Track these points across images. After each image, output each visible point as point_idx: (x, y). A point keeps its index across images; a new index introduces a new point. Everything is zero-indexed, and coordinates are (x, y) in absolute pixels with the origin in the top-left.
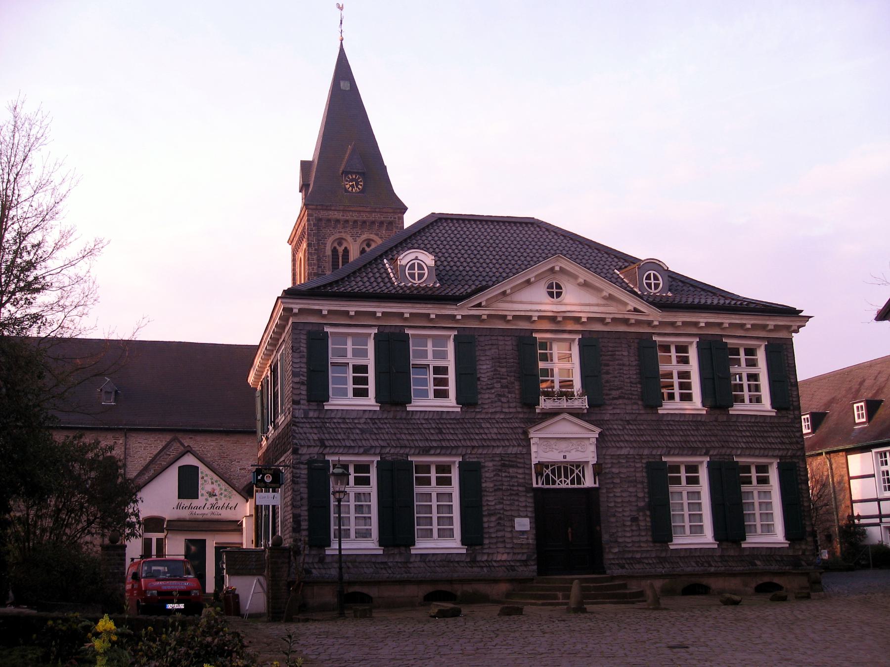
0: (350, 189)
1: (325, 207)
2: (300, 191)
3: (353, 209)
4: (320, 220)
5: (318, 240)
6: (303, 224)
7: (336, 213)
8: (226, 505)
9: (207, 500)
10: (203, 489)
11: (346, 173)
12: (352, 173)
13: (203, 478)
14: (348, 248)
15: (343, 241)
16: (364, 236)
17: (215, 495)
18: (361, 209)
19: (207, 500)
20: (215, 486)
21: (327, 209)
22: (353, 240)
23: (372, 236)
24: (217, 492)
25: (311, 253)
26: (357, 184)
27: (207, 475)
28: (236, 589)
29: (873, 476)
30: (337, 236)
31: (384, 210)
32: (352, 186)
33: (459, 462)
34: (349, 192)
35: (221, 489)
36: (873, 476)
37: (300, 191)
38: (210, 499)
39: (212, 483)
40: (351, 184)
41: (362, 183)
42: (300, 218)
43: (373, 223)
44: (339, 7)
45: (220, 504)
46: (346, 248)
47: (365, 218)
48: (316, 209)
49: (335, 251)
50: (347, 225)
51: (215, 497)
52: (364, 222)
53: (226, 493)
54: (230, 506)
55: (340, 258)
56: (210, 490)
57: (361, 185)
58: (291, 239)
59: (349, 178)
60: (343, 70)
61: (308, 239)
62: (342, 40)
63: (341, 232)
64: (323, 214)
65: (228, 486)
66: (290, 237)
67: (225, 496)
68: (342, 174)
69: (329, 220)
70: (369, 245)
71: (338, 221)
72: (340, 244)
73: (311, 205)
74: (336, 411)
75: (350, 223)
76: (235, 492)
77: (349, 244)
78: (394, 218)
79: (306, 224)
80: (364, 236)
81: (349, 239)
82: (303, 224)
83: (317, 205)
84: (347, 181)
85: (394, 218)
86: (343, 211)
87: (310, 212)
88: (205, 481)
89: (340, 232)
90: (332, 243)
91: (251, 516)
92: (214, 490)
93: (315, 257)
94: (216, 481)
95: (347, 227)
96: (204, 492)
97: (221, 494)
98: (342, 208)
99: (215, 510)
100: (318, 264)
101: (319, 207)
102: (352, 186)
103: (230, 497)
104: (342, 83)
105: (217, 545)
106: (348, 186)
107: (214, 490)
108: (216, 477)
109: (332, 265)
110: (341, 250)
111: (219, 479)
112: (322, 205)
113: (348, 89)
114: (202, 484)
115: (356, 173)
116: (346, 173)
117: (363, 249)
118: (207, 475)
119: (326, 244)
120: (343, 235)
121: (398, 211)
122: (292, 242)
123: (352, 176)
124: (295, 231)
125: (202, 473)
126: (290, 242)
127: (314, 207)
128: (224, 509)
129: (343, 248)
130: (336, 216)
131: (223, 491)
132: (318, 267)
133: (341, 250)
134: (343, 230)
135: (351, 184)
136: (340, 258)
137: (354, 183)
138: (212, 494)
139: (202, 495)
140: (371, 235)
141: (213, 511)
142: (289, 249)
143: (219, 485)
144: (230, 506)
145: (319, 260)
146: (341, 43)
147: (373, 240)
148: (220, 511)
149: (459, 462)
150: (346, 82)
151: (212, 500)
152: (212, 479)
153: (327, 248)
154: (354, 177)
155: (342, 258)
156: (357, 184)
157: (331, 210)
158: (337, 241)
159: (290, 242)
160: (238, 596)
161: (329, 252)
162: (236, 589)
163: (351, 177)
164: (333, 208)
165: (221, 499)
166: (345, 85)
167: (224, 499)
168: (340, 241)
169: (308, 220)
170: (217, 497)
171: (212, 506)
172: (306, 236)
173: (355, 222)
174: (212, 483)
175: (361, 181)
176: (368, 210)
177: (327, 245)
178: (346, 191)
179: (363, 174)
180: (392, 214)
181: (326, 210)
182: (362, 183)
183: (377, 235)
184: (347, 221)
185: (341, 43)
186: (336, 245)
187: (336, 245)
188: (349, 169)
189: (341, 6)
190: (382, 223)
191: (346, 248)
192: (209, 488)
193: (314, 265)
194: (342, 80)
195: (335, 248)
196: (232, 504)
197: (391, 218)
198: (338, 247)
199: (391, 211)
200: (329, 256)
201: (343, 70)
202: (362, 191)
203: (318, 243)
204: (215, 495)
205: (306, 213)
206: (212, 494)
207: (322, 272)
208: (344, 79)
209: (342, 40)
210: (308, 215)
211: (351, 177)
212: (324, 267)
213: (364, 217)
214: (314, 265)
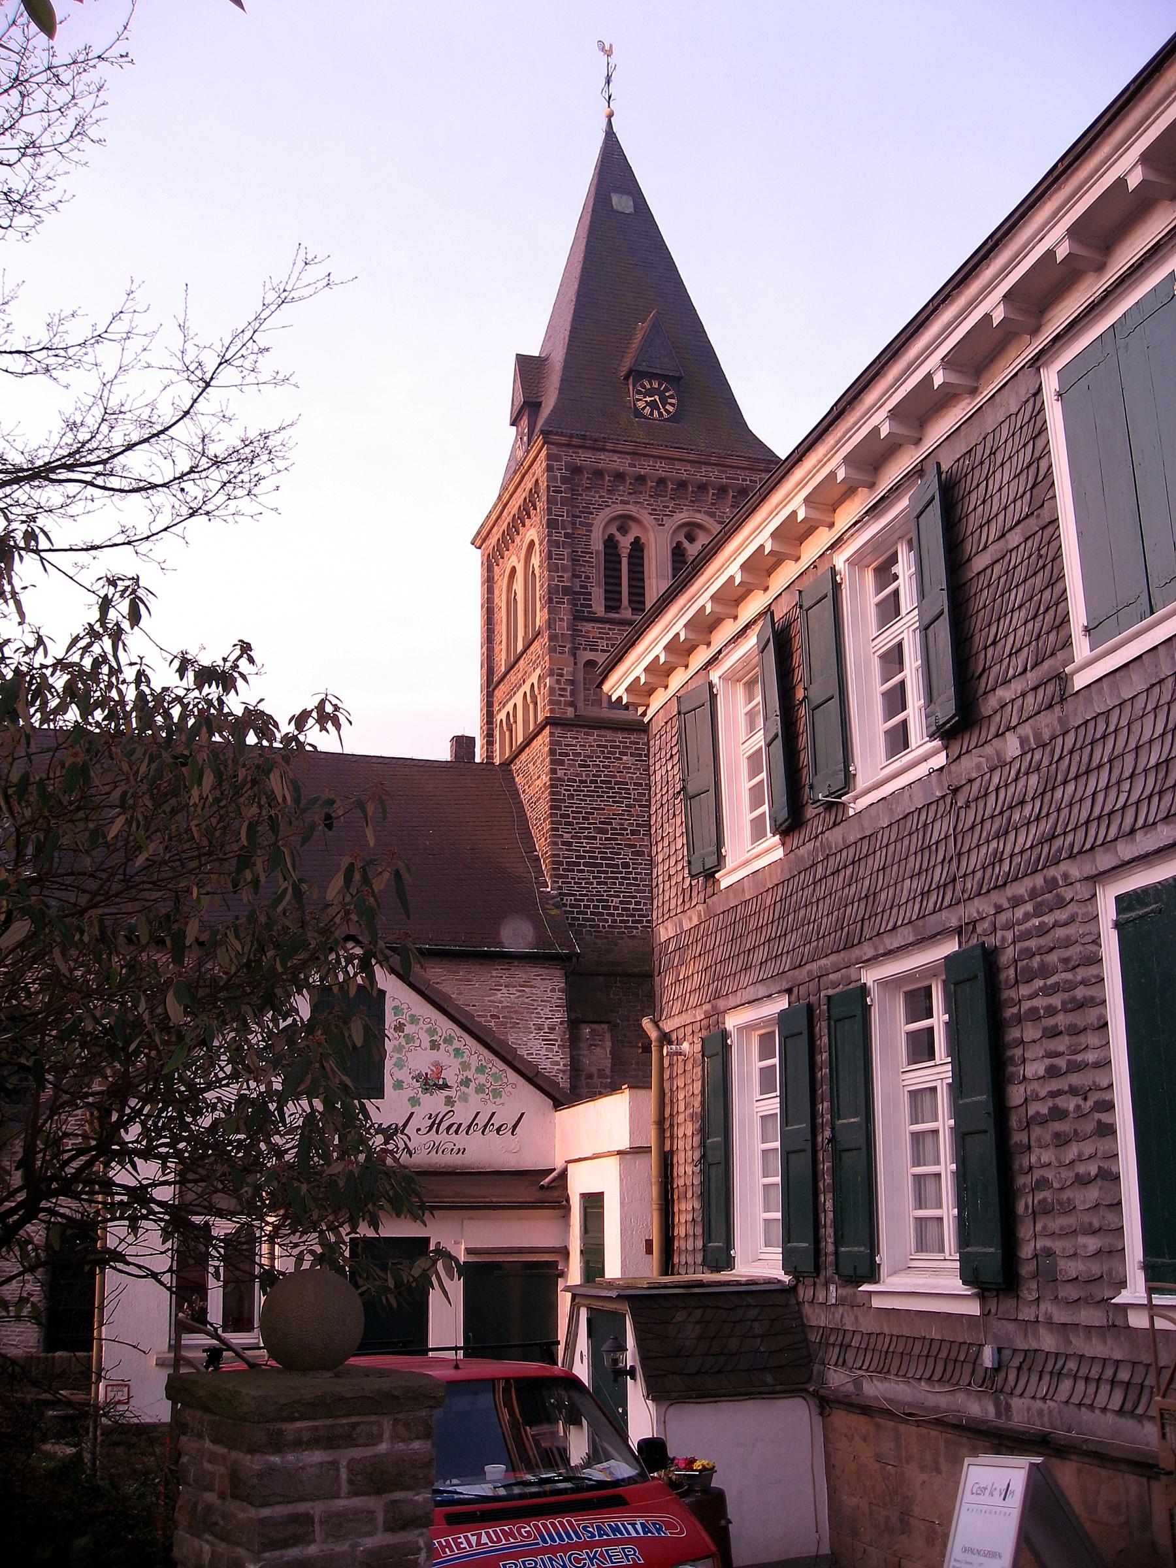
1: (589, 443)
2: (512, 424)
3: (655, 452)
4: (577, 470)
5: (573, 516)
6: (528, 484)
7: (616, 458)
8: (481, 1120)
9: (414, 1101)
10: (399, 1065)
11: (636, 374)
12: (651, 376)
13: (399, 1028)
15: (633, 525)
17: (445, 1086)
19: (414, 1101)
20: (443, 1056)
21: (597, 447)
22: (654, 522)
23: (700, 518)
25: (557, 542)
26: (664, 402)
27: (414, 1020)
28: (712, 1470)
29: (985, 1132)
30: (619, 510)
31: (728, 462)
32: (653, 405)
34: (646, 417)
35: (465, 1066)
36: (985, 1132)
37: (512, 424)
38: (425, 1098)
39: (434, 1046)
40: (648, 399)
42: (517, 471)
43: (703, 487)
44: (603, 49)
45: (462, 1115)
47: (684, 476)
48: (569, 445)
49: (611, 544)
50: (641, 488)
51: (445, 1093)
52: (682, 484)
53: (482, 1079)
57: (672, 404)
58: (484, 532)
59: (643, 386)
60: (247, 682)
63: (627, 503)
64: (584, 458)
65: (491, 1056)
66: (482, 526)
67: (480, 1089)
68: (627, 378)
69: (599, 473)
70: (691, 539)
71: (619, 476)
72: (623, 530)
73: (557, 434)
74: (907, 793)
75: (650, 484)
76: (513, 1076)
77: (645, 530)
78: (751, 481)
79: (543, 485)
80: (683, 516)
81: (647, 519)
83: (571, 436)
84: (639, 392)
85: (751, 481)
87: (555, 450)
88: (409, 1039)
89: (623, 502)
90: (606, 526)
91: (636, 1151)
93: (566, 552)
94: (448, 1040)
95: (641, 493)
96: (403, 1075)
97: (466, 1082)
98: (629, 449)
99: (443, 1137)
101: (575, 441)
102: (653, 405)
104: (615, 199)
105: (472, 1259)
106: (641, 404)
107: (439, 1068)
108: (446, 1026)
109: (605, 576)
110: (625, 542)
112: (584, 437)
114: (398, 1049)
115: (661, 378)
116: (636, 374)
118: (414, 1020)
119: (591, 525)
120: (632, 510)
121: (762, 466)
122: (484, 541)
123: (651, 385)
124: (499, 508)
126: (479, 540)
127: (563, 440)
129: (630, 538)
130: (615, 465)
132: (574, 576)
133: (625, 542)
134: (632, 499)
135: (648, 399)
138: (432, 1083)
140: (698, 515)
141: (437, 1139)
142: (475, 557)
143: (457, 1051)
145: (574, 560)
146: (610, 123)
147: (700, 526)
148: (461, 1140)
151: (434, 1103)
152: (432, 1032)
153: (593, 535)
156: (664, 402)
158: (618, 522)
159: (478, 542)
160: (719, 1498)
161: (597, 545)
162: (712, 1470)
163: (648, 386)
164: (609, 446)
165: (465, 1098)
166: (623, 203)
168: (624, 522)
169: (549, 468)
170: (452, 1093)
171: (435, 1124)
172: (541, 505)
173: (661, 482)
174: (434, 1046)
175: (671, 397)
176: (692, 457)
178: (638, 413)
180: (747, 472)
183: (712, 515)
184: (641, 479)
185: (610, 123)
186: (613, 530)
188: (643, 368)
189: (607, 47)
190: (723, 490)
191: (637, 539)
192: (422, 1060)
193: (564, 569)
195: (611, 537)
196: (506, 1116)
197: (743, 480)
198: (618, 537)
199: (746, 464)
200: (597, 552)
201: (247, 682)
202: (674, 418)
203: (574, 524)
204: (445, 1086)
205: (544, 452)
206: (432, 1083)
209: (610, 116)
210: (549, 457)
211: (648, 386)
212: (587, 577)
213: (683, 472)
214: (564, 569)
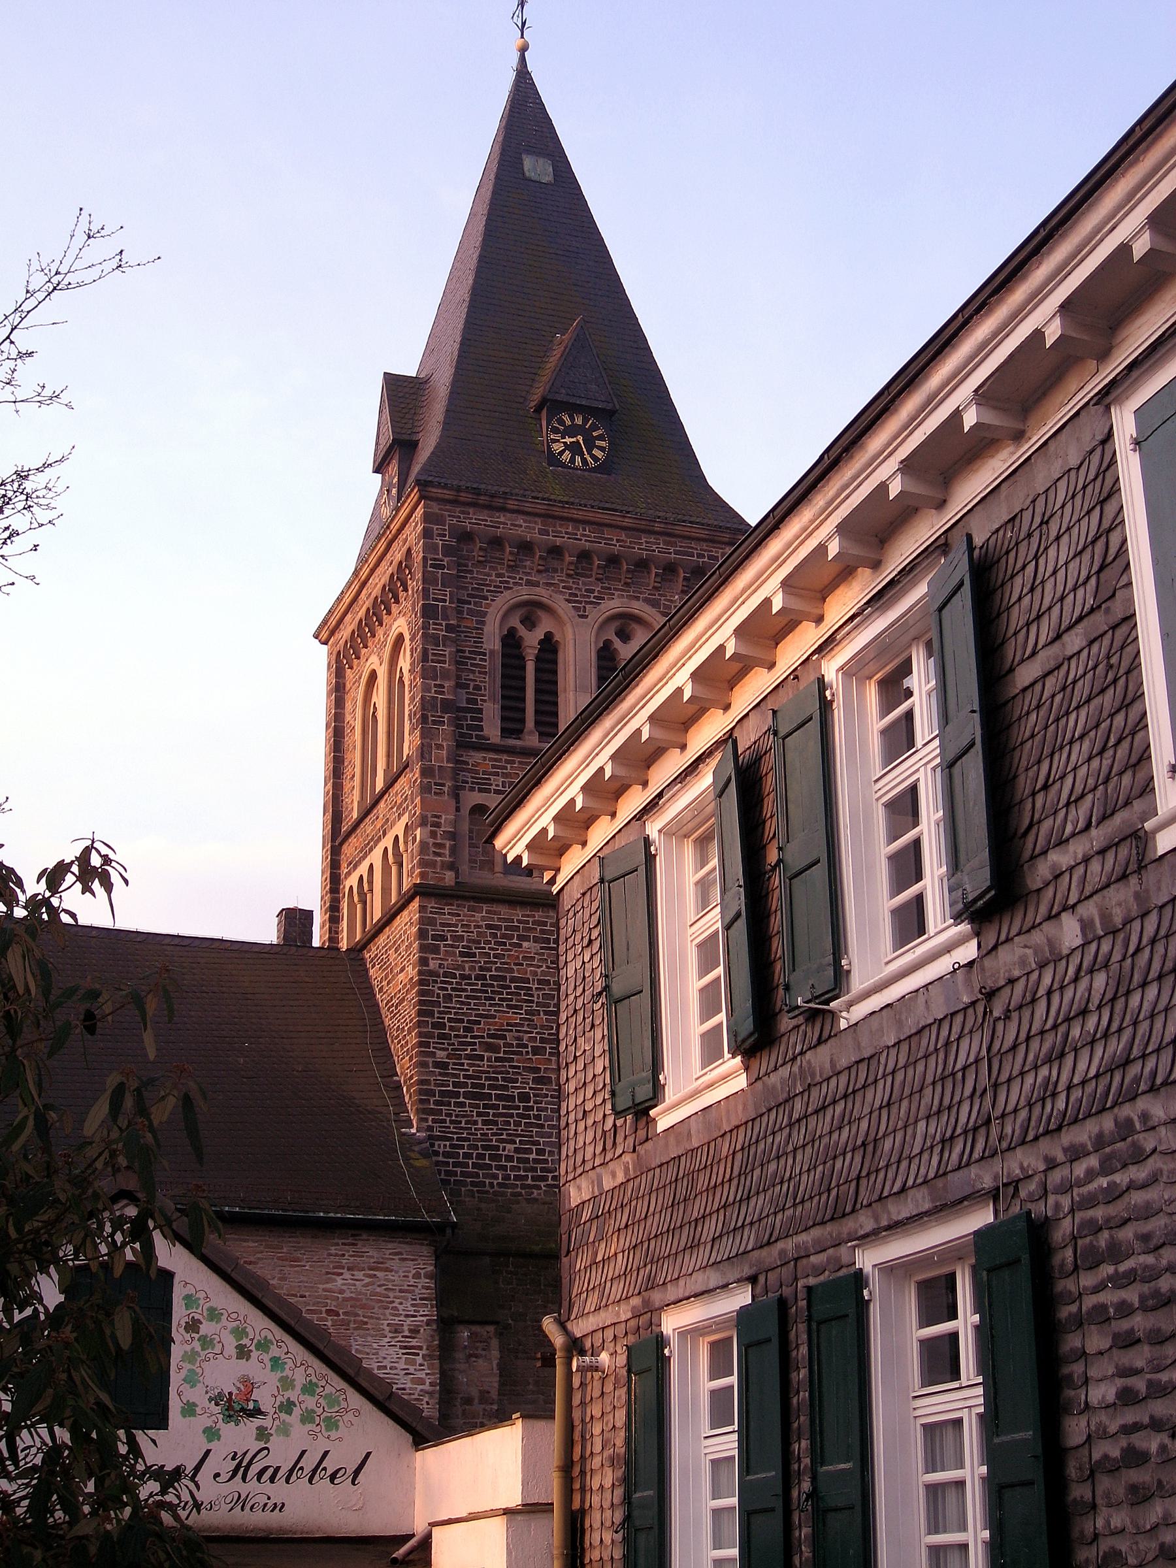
0: (567, 456)
1: (483, 499)
3: (579, 515)
4: (466, 537)
5: (459, 601)
6: (397, 553)
8: (308, 1463)
9: (211, 1433)
10: (191, 1380)
11: (552, 405)
12: (573, 409)
13: (193, 1326)
14: (557, 637)
15: (540, 613)
16: (614, 605)
17: (257, 1412)
18: (605, 517)
19: (211, 1433)
20: (254, 1368)
23: (638, 607)
24: (264, 1397)
30: (524, 593)
31: (678, 530)
32: (574, 448)
33: (162, 1422)
35: (287, 1383)
37: (377, 470)
38: (228, 1430)
39: (243, 1353)
40: (568, 440)
41: (603, 444)
43: (642, 565)
45: (281, 1454)
46: (549, 636)
47: (616, 549)
48: (455, 502)
49: (511, 641)
51: (257, 1422)
52: (613, 560)
53: (310, 1402)
54: (330, 1465)
55: (530, 667)
56: (228, 1386)
57: (602, 449)
58: (333, 622)
59: (562, 422)
61: (425, 593)
62: (523, 49)
63: (536, 584)
64: (475, 520)
67: (308, 1417)
68: (538, 410)
69: (496, 542)
71: (526, 547)
72: (530, 622)
75: (568, 559)
76: (355, 1400)
80: (614, 605)
82: (397, 553)
84: (555, 431)
86: (546, 516)
87: (435, 508)
88: (206, 1342)
89: (530, 583)
90: (505, 617)
91: (531, 1509)
92: (249, 1385)
93: (448, 651)
94: (263, 1346)
95: (555, 571)
96: (197, 1395)
97: (287, 1407)
98: (541, 508)
100: (458, 677)
101: (464, 497)
102: (574, 448)
103: (331, 1424)
104: (528, 163)
106: (557, 447)
107: (249, 1385)
108: (259, 1324)
109: (502, 687)
110: (532, 639)
111: (279, 1333)
112: (477, 492)
113: (548, 178)
114: (190, 1357)
116: (552, 405)
117: (607, 644)
118: (214, 1315)
120: (542, 593)
123: (572, 419)
125: (189, 1300)
126: (326, 632)
127: (448, 494)
128: (300, 1484)
129: (539, 634)
131: (293, 1395)
132: (459, 686)
133: (532, 639)
135: (568, 440)
136: (530, 667)
137: (580, 438)
139: (189, 1410)
141: (244, 1489)
142: (319, 657)
144: (330, 1465)
145: (460, 661)
146: (523, 59)
147: (638, 620)
148: (278, 1491)
149: (162, 1422)
150: (541, 161)
152: (239, 1333)
154: (579, 421)
155: (537, 670)
157: (503, 509)
159: (324, 635)
161: (492, 641)
165: (285, 1430)
166: (536, 168)
167: (299, 1431)
168: (531, 612)
169: (427, 534)
170: (267, 1422)
171: (241, 1468)
172: (415, 584)
173: (585, 556)
174: (243, 1353)
176: (627, 522)
177: (489, 619)
178: (553, 459)
179: (605, 415)
180: (704, 545)
181: (489, 507)
182: (603, 444)
183: (654, 604)
184: (556, 551)
185: (523, 59)
186: (515, 621)
187: (515, 621)
190: (670, 569)
191: (549, 636)
193: (445, 675)
194: (528, 152)
195: (512, 632)
196: (343, 1457)
197: (700, 556)
198: (522, 631)
200: (492, 652)
202: (604, 468)
203: (460, 612)
204: (257, 1412)
205: (420, 511)
207: (469, 701)
208: (532, 150)
209: (523, 49)
210: (427, 518)
212: (477, 688)
213: (615, 543)
214: (445, 675)
